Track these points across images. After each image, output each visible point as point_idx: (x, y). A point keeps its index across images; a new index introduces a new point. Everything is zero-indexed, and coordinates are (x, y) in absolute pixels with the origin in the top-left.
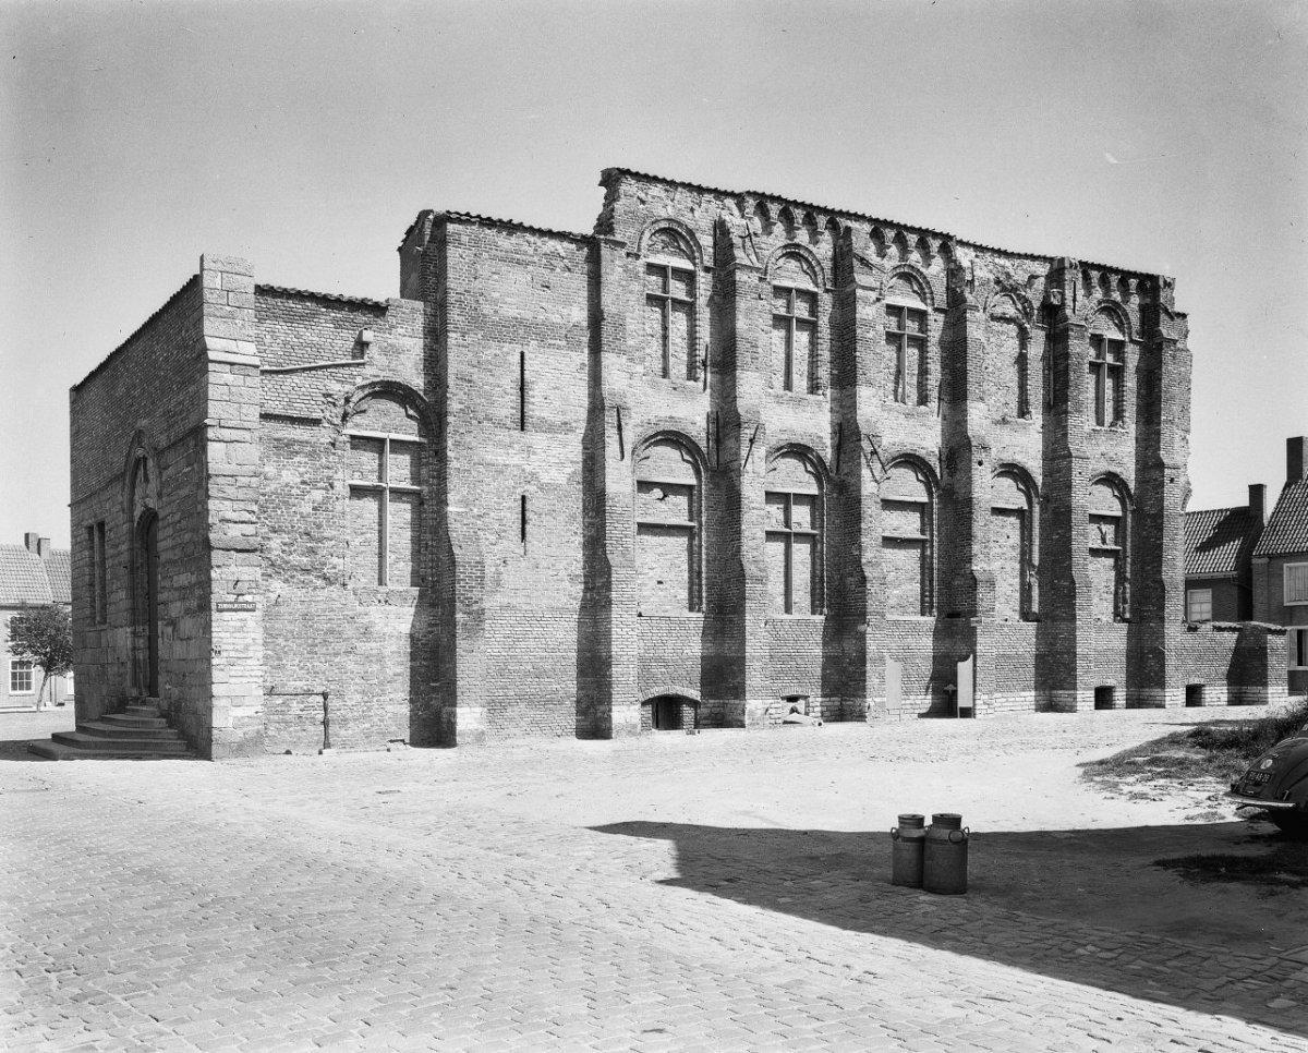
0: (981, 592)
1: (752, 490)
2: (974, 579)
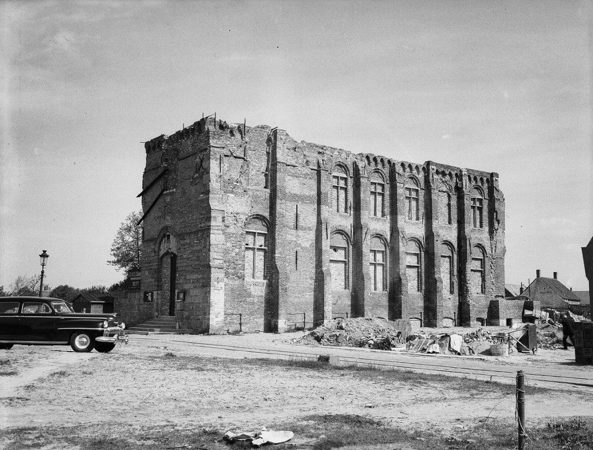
0: (438, 284)
1: (365, 250)
2: (435, 279)
